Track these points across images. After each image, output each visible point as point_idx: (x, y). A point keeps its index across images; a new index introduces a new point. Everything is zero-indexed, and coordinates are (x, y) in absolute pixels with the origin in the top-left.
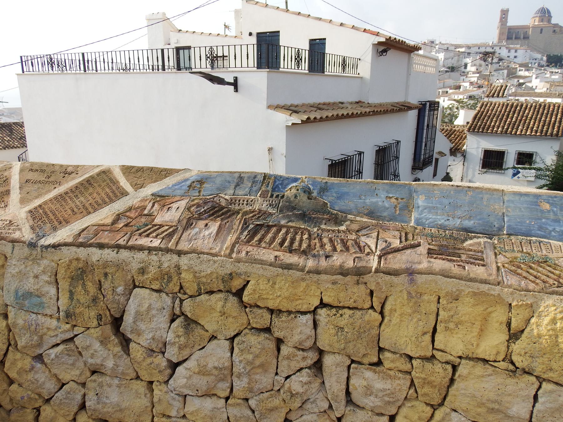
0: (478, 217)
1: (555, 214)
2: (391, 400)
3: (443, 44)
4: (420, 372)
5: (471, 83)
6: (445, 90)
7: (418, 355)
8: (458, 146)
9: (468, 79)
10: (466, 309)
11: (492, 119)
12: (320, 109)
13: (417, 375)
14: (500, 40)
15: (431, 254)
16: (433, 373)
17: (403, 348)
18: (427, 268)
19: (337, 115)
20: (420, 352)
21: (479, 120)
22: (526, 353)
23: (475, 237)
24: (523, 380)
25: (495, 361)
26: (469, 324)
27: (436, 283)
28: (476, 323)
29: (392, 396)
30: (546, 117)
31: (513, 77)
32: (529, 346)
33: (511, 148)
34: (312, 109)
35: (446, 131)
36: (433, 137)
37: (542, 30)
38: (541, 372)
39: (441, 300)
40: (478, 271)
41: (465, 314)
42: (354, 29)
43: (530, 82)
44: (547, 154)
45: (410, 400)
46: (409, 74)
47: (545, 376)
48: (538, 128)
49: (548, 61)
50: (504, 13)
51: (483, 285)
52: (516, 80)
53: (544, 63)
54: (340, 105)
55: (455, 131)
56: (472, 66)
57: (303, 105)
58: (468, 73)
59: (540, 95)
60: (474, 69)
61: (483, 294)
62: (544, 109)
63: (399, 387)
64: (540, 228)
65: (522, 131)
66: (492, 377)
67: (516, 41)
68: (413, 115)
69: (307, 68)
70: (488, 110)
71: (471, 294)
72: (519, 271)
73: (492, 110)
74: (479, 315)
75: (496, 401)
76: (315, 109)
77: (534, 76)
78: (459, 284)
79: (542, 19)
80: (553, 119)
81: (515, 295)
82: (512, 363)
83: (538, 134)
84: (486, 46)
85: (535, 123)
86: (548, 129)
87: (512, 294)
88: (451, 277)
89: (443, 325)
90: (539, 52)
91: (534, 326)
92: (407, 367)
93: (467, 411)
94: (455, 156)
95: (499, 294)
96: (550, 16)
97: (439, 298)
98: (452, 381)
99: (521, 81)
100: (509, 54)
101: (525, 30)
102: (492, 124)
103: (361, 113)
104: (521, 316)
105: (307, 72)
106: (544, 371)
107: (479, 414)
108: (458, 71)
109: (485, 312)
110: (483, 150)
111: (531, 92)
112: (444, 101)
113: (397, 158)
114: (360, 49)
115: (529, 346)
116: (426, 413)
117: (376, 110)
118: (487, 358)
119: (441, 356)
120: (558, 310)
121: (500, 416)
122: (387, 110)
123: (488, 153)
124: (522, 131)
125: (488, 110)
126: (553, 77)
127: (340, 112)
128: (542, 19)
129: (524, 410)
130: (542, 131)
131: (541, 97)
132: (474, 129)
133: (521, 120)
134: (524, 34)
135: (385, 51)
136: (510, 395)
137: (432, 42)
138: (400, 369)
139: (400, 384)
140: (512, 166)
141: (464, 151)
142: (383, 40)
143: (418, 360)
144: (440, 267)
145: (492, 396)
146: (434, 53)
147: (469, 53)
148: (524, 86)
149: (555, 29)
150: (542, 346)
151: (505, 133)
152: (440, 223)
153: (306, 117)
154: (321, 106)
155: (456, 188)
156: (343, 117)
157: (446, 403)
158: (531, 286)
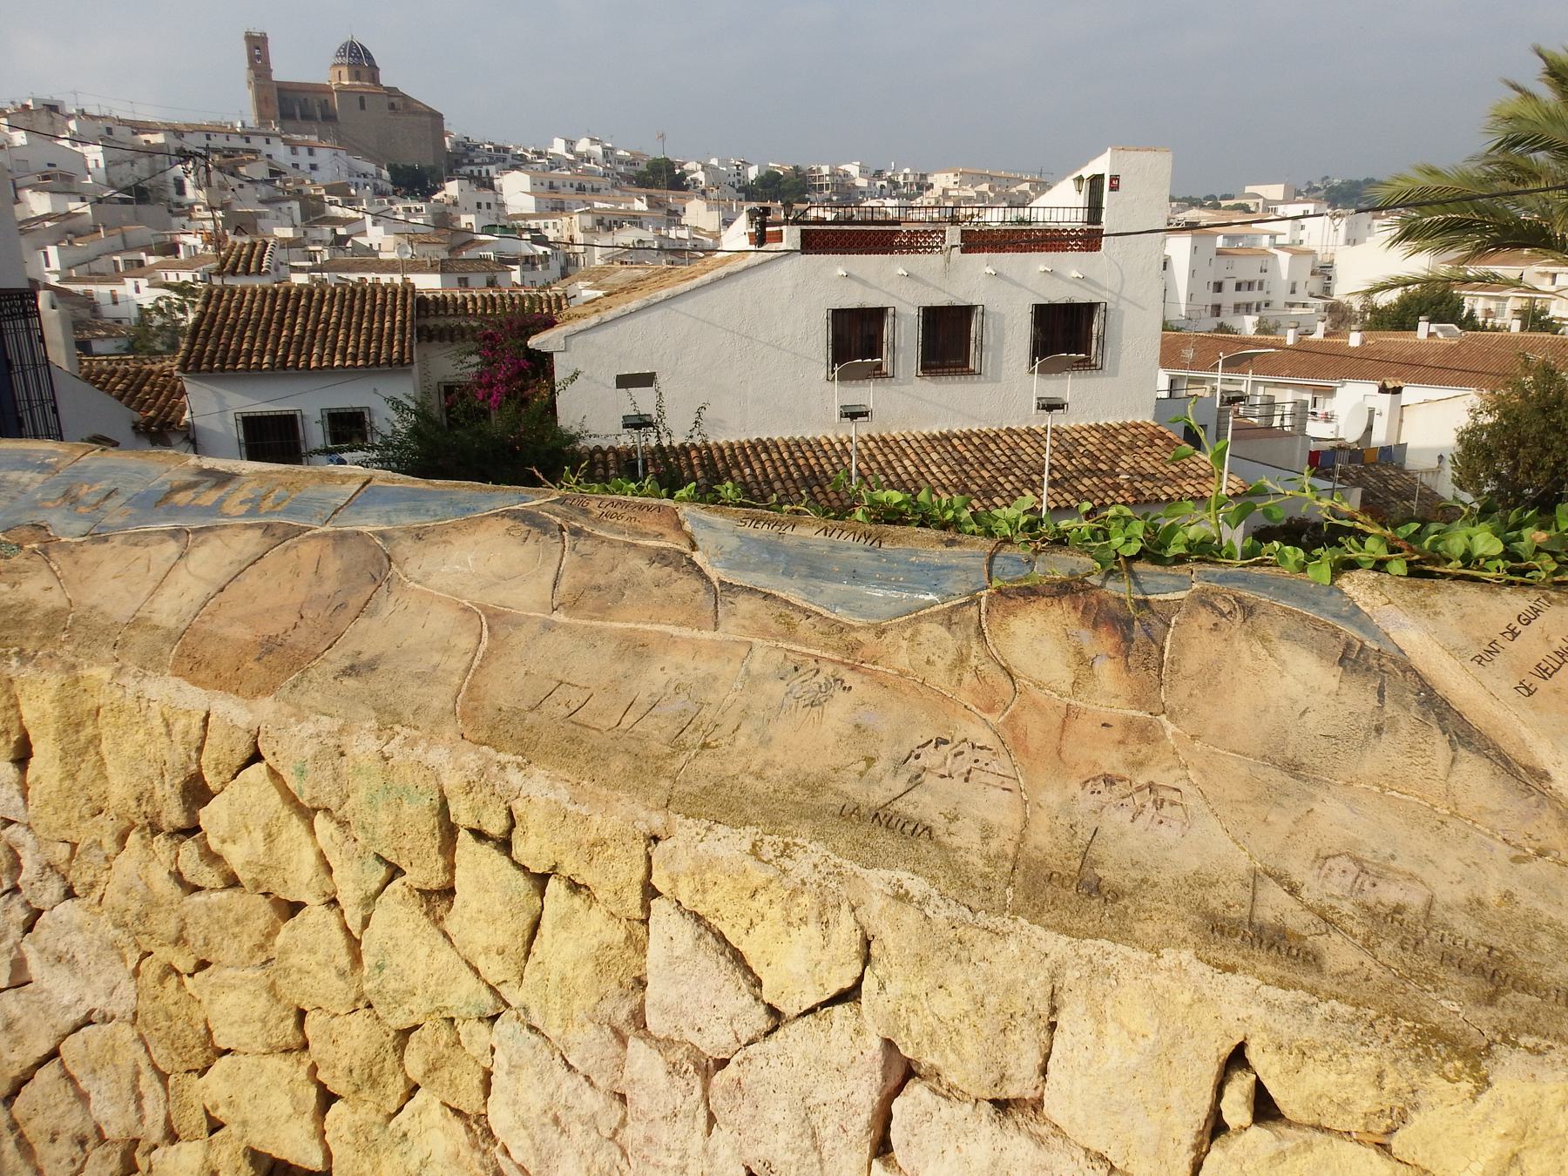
3: (93, 117)
8: (169, 414)
11: (243, 332)
14: (261, 115)
30: (371, 322)
33: (309, 403)
35: (124, 377)
36: (46, 395)
37: (362, 100)
43: (363, 233)
44: (386, 402)
48: (357, 347)
49: (394, 182)
50: (257, 46)
52: (327, 229)
55: (151, 372)
58: (191, 206)
59: (390, 267)
62: (363, 301)
70: (228, 310)
77: (369, 219)
80: (387, 325)
83: (360, 363)
84: (229, 133)
85: (348, 337)
86: (379, 348)
90: (371, 158)
94: (168, 444)
99: (341, 231)
100: (295, 159)
101: (324, 97)
102: (245, 346)
108: (159, 199)
110: (239, 417)
111: (369, 259)
112: (137, 290)
124: (320, 359)
125: (228, 310)
131: (395, 271)
132: (198, 364)
133: (314, 332)
134: (321, 106)
137: (53, 108)
141: (188, 425)
148: (349, 244)
149: (394, 100)
151: (281, 369)
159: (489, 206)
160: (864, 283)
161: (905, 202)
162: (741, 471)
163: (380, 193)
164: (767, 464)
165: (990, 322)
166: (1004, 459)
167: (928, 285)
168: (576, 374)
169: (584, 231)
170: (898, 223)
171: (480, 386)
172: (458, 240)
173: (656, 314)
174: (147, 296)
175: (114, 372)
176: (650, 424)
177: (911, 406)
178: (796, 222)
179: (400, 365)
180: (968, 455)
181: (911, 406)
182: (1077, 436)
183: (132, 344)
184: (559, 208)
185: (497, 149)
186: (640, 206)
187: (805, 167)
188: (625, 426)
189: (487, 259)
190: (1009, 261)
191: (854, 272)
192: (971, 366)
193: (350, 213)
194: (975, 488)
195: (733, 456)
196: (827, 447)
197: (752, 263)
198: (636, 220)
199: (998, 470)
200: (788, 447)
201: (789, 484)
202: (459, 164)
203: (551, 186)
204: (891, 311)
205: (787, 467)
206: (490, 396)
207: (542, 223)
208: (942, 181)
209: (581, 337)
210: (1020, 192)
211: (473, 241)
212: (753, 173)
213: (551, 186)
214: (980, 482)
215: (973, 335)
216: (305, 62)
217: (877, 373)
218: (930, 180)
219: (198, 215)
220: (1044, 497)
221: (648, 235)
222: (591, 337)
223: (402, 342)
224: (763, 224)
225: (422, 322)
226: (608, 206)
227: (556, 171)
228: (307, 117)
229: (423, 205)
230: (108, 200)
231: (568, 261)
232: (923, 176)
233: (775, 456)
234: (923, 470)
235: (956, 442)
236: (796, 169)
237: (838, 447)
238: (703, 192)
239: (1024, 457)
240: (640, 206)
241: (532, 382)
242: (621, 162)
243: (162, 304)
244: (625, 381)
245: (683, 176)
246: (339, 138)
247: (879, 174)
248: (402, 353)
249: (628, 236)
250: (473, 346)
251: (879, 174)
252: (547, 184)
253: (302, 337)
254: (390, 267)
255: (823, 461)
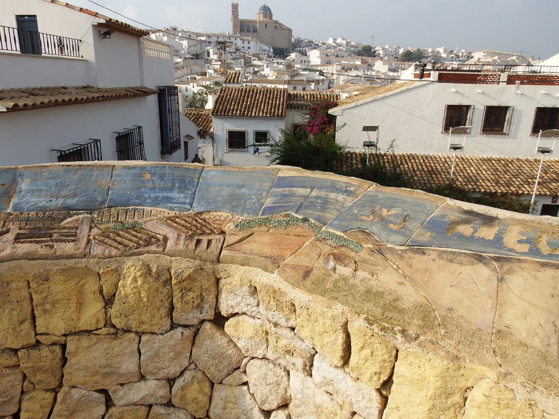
0: (83, 194)
1: (153, 182)
2: (5, 399)
3: (185, 32)
4: (26, 362)
5: (215, 71)
6: (193, 76)
7: (20, 345)
9: (212, 67)
10: (59, 287)
12: (33, 95)
13: (24, 366)
15: (19, 239)
16: (41, 358)
17: (3, 343)
18: (9, 254)
19: (56, 101)
20: (22, 342)
21: (220, 104)
22: (121, 314)
23: (76, 214)
24: (125, 338)
25: (97, 329)
26: (65, 301)
27: (21, 267)
28: (72, 299)
29: (4, 395)
30: (273, 101)
31: (249, 66)
32: (122, 307)
33: (250, 128)
34: (23, 94)
37: (266, 25)
38: (136, 327)
39: (31, 285)
40: (68, 248)
41: (58, 293)
42: (69, 7)
43: (263, 70)
44: (276, 131)
45: (28, 392)
46: (141, 59)
47: (140, 330)
49: (274, 53)
50: (235, 7)
51: (70, 260)
52: (252, 68)
53: (272, 55)
54: (63, 90)
55: (202, 114)
56: (213, 54)
57: (11, 90)
58: (211, 60)
59: (271, 82)
60: (215, 57)
61: (71, 269)
63: (11, 384)
64: (138, 197)
65: (255, 113)
66: (99, 345)
67: (248, 34)
68: (152, 100)
69: (18, 49)
71: (59, 271)
72: (107, 240)
73: (230, 95)
74: (73, 290)
75: (107, 366)
76: (27, 95)
77: (265, 66)
78: (45, 264)
79: (266, 16)
81: (101, 263)
82: (114, 326)
87: (97, 263)
88: (36, 259)
89: (39, 308)
90: (267, 45)
91: (121, 289)
92: (13, 360)
93: (84, 383)
94: (205, 138)
95: (86, 266)
96: (271, 14)
97: (29, 283)
98: (64, 360)
99: (256, 69)
100: (243, 45)
101: (254, 24)
103: (87, 98)
104: (109, 282)
105: (19, 53)
106: (138, 325)
107: (97, 382)
108: (202, 58)
109: (77, 286)
111: (264, 78)
112: (193, 87)
113: (141, 143)
114: (81, 30)
115: (122, 307)
116: (47, 399)
117: (105, 95)
118: (89, 328)
119: (45, 340)
120: (137, 269)
121: (115, 377)
122: (120, 95)
123: (232, 134)
124: (255, 113)
126: (279, 66)
127: (60, 98)
128: (266, 16)
129: (133, 365)
130: (270, 113)
131: (272, 83)
132: (217, 113)
133: (254, 104)
135: (107, 34)
136: (118, 356)
138: (5, 365)
139: (10, 381)
140: (252, 144)
141: (212, 133)
142: (103, 21)
143: (22, 350)
144: (24, 251)
145: (103, 362)
146: (177, 40)
147: (210, 42)
149: (276, 25)
150: (130, 304)
151: (243, 116)
152: (41, 205)
153: (12, 104)
154: (35, 91)
155: (67, 167)
156: (64, 103)
157: (64, 383)
158: (114, 252)
159: (305, 61)
160: (462, 95)
161: (461, 63)
162: (404, 166)
163: (269, 57)
164: (414, 164)
165: (515, 114)
166: (515, 171)
167: (490, 97)
168: (345, 125)
169: (337, 71)
170: (480, 71)
171: (309, 126)
172: (294, 74)
173: (377, 103)
174: (196, 89)
175: (191, 113)
176: (373, 145)
177: (478, 146)
178: (437, 70)
179: (281, 117)
180: (499, 168)
181: (478, 146)
182: (549, 164)
183: (190, 104)
184: (329, 63)
185: (309, 42)
186: (358, 63)
187: (422, 49)
188: (364, 145)
189: (303, 80)
190: (528, 89)
191: (459, 91)
192: (504, 131)
193: (259, 63)
194: (502, 182)
195: (401, 160)
196: (438, 159)
197: (417, 85)
198: (356, 68)
199: (513, 175)
200: (423, 158)
201: (423, 173)
202: (296, 47)
203: (327, 55)
204: (472, 107)
205: (422, 166)
206: (312, 130)
207: (322, 68)
208: (478, 55)
209: (348, 111)
210: (512, 60)
211: (299, 74)
212: (401, 51)
213: (327, 55)
214: (505, 180)
215: (507, 118)
216: (250, 13)
217: (464, 132)
218: (473, 55)
219: (213, 63)
220: (535, 189)
221: (360, 73)
222: (351, 111)
223: (282, 109)
224: (423, 70)
225: (288, 102)
226: (347, 62)
227: (329, 50)
228: (248, 31)
229: (283, 61)
230: (188, 58)
231: (330, 82)
232: (470, 53)
233: (417, 161)
234: (479, 172)
235: (494, 162)
236: (418, 50)
237: (443, 160)
238: (382, 58)
239: (524, 171)
240: (358, 63)
241: (327, 126)
242: (352, 47)
243: (200, 92)
244: (366, 129)
245: (375, 52)
246: (257, 38)
247: (451, 52)
248: (282, 113)
249: (354, 73)
250: (308, 112)
251: (451, 52)
252: (325, 54)
253: (250, 105)
254: (271, 82)
255: (437, 165)
